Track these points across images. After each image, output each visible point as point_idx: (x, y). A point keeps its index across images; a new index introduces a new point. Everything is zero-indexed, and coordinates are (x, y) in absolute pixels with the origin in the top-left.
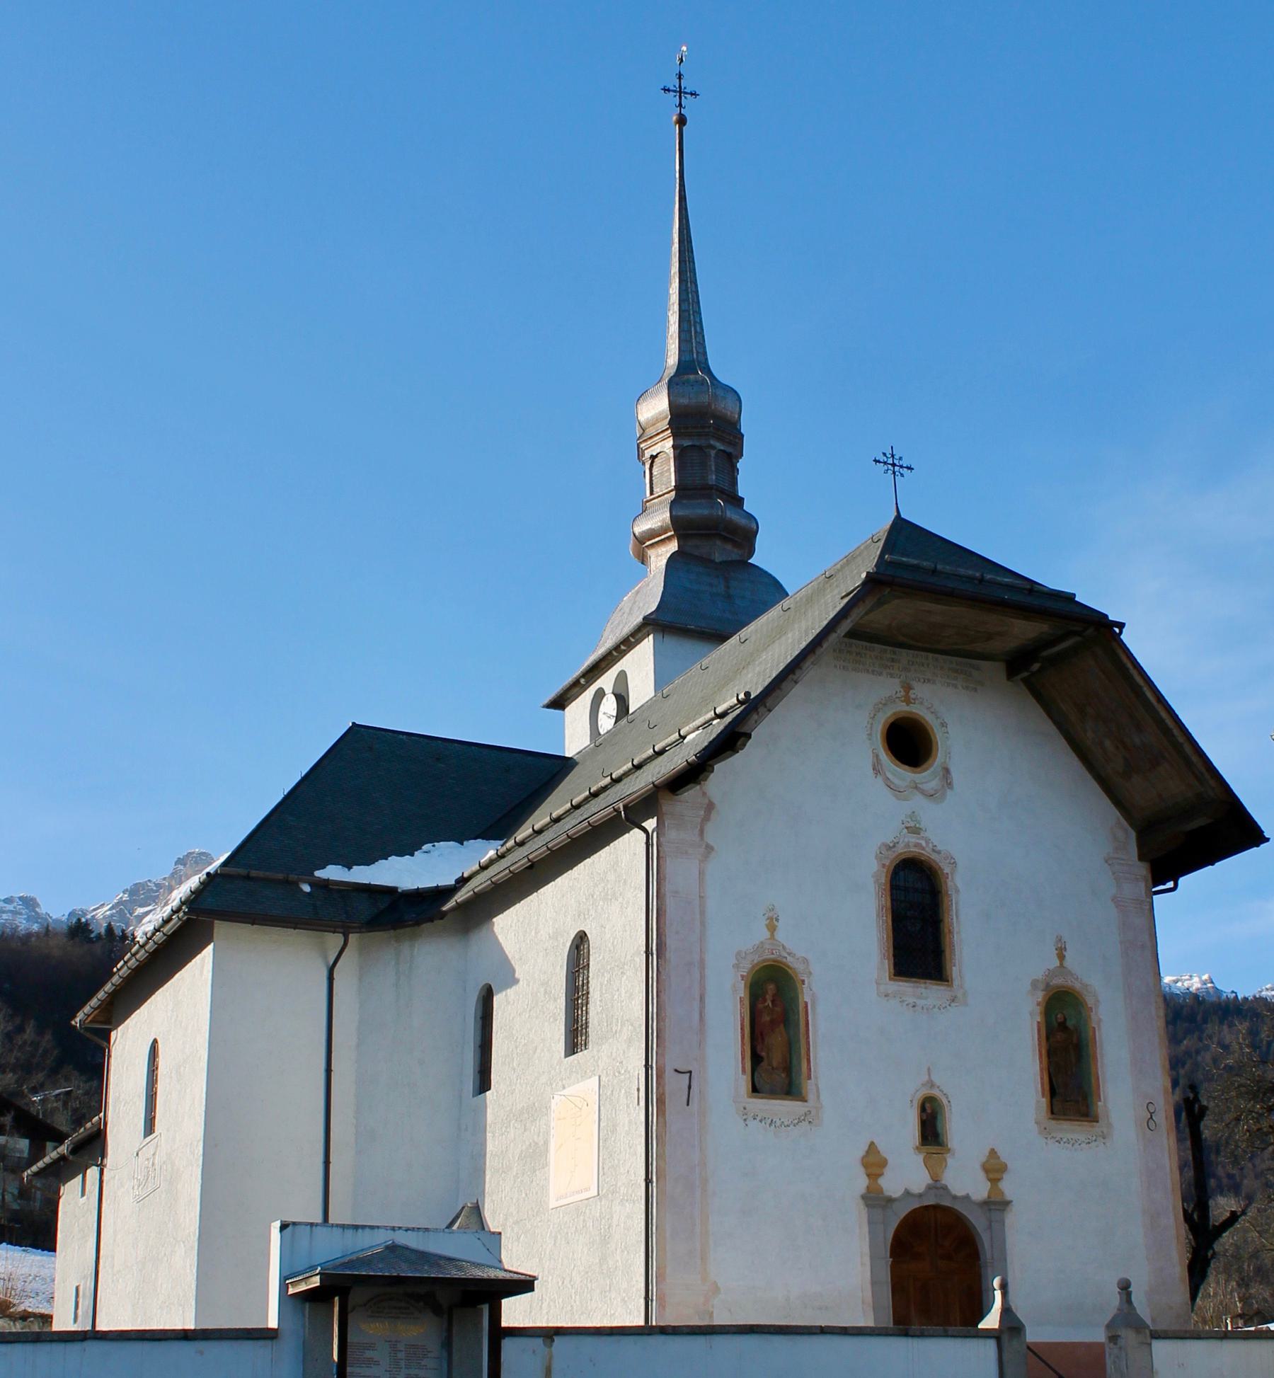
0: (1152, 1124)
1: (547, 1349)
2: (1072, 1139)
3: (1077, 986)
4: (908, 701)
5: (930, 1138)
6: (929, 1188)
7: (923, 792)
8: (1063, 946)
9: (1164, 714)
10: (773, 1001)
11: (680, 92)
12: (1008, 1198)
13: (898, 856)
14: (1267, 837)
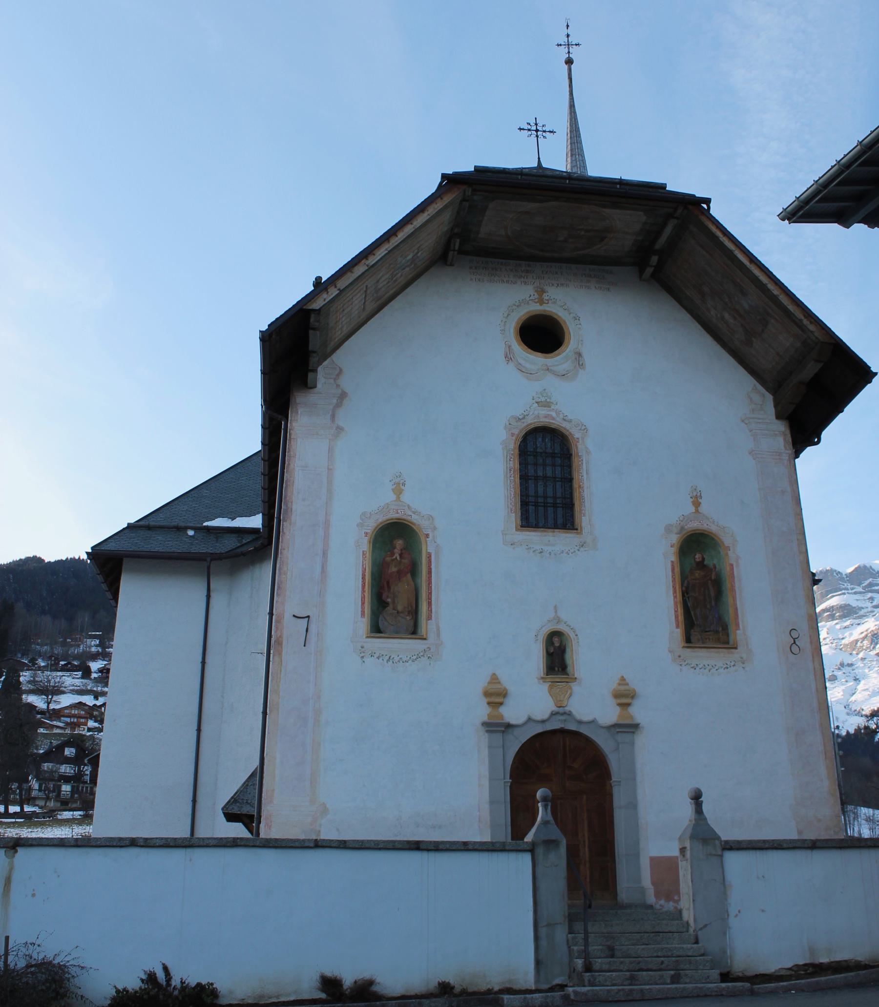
0: (795, 648)
1: (7, 860)
2: (715, 665)
3: (713, 529)
4: (541, 302)
5: (556, 669)
6: (553, 714)
7: (555, 373)
8: (699, 494)
9: (757, 272)
10: (401, 555)
11: (568, 45)
12: (638, 721)
13: (528, 426)
14: (874, 371)
